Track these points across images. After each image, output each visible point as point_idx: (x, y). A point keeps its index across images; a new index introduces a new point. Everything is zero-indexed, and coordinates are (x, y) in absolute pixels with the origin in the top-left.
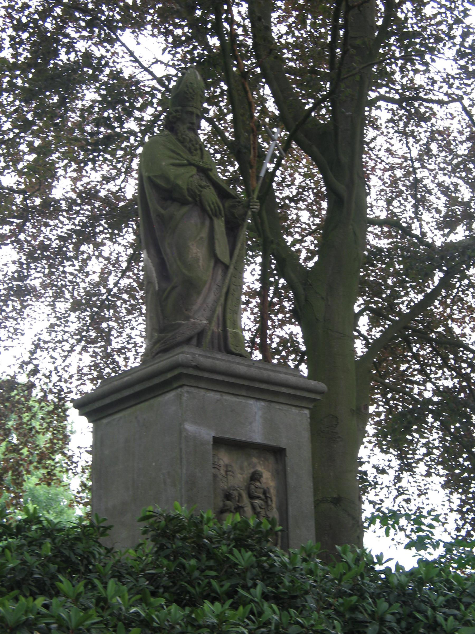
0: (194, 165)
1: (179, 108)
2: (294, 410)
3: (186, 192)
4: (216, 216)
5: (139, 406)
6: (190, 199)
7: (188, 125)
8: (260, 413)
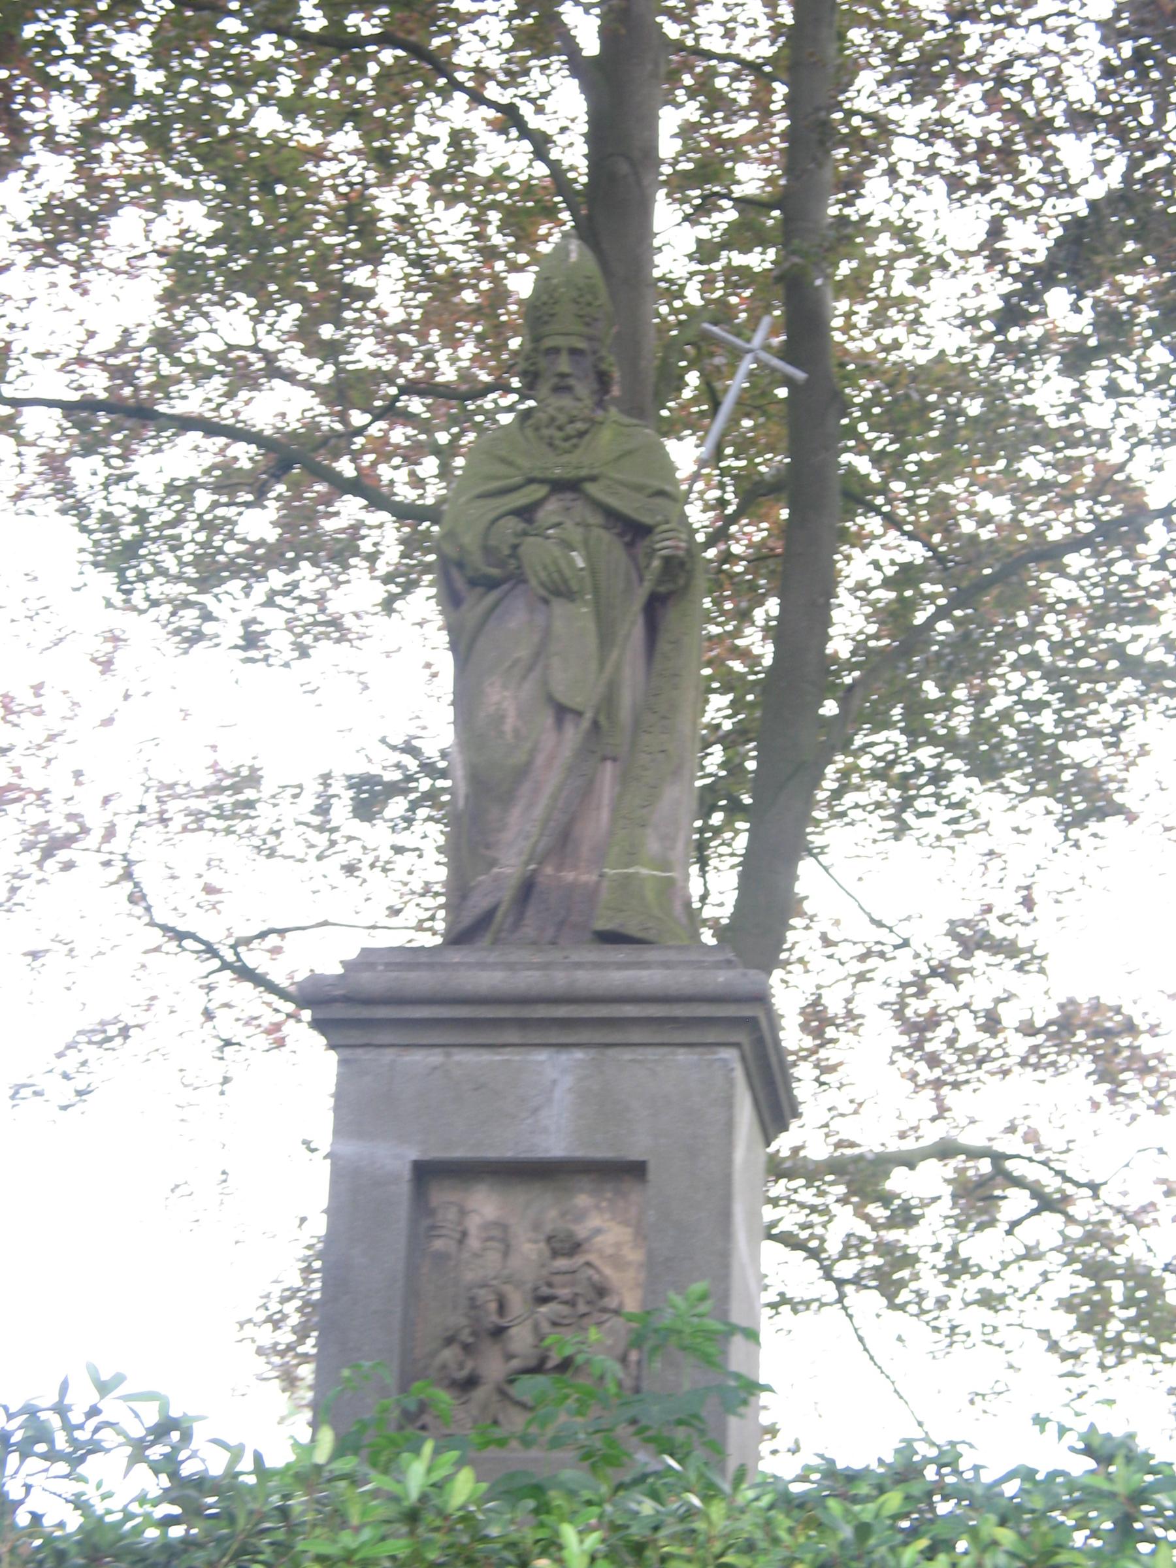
2: (683, 1056)
7: (555, 380)
8: (567, 1081)
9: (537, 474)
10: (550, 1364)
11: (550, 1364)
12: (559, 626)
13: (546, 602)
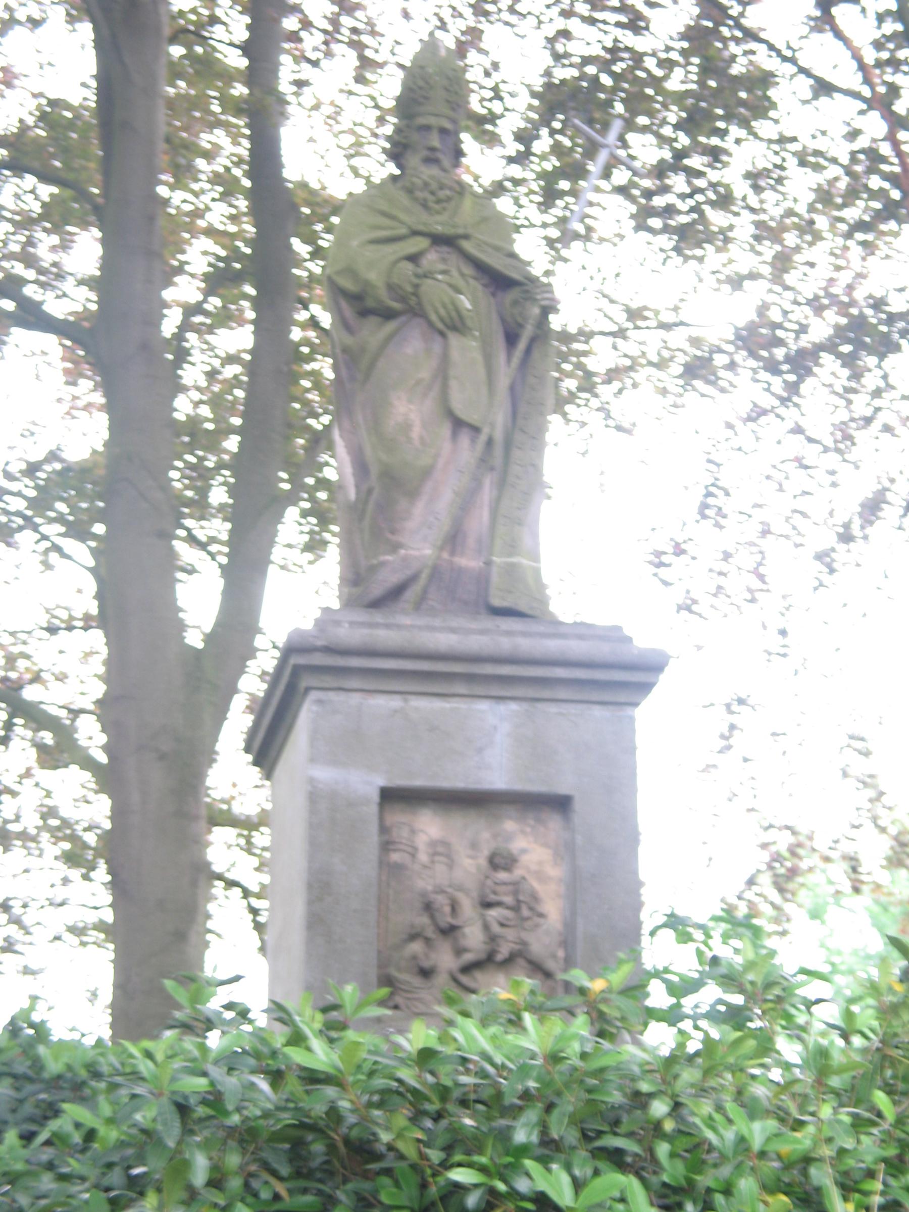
2: (598, 712)
7: (425, 153)
8: (505, 728)
9: (421, 228)
10: (499, 957)
11: (499, 957)
12: (455, 355)
13: (442, 334)
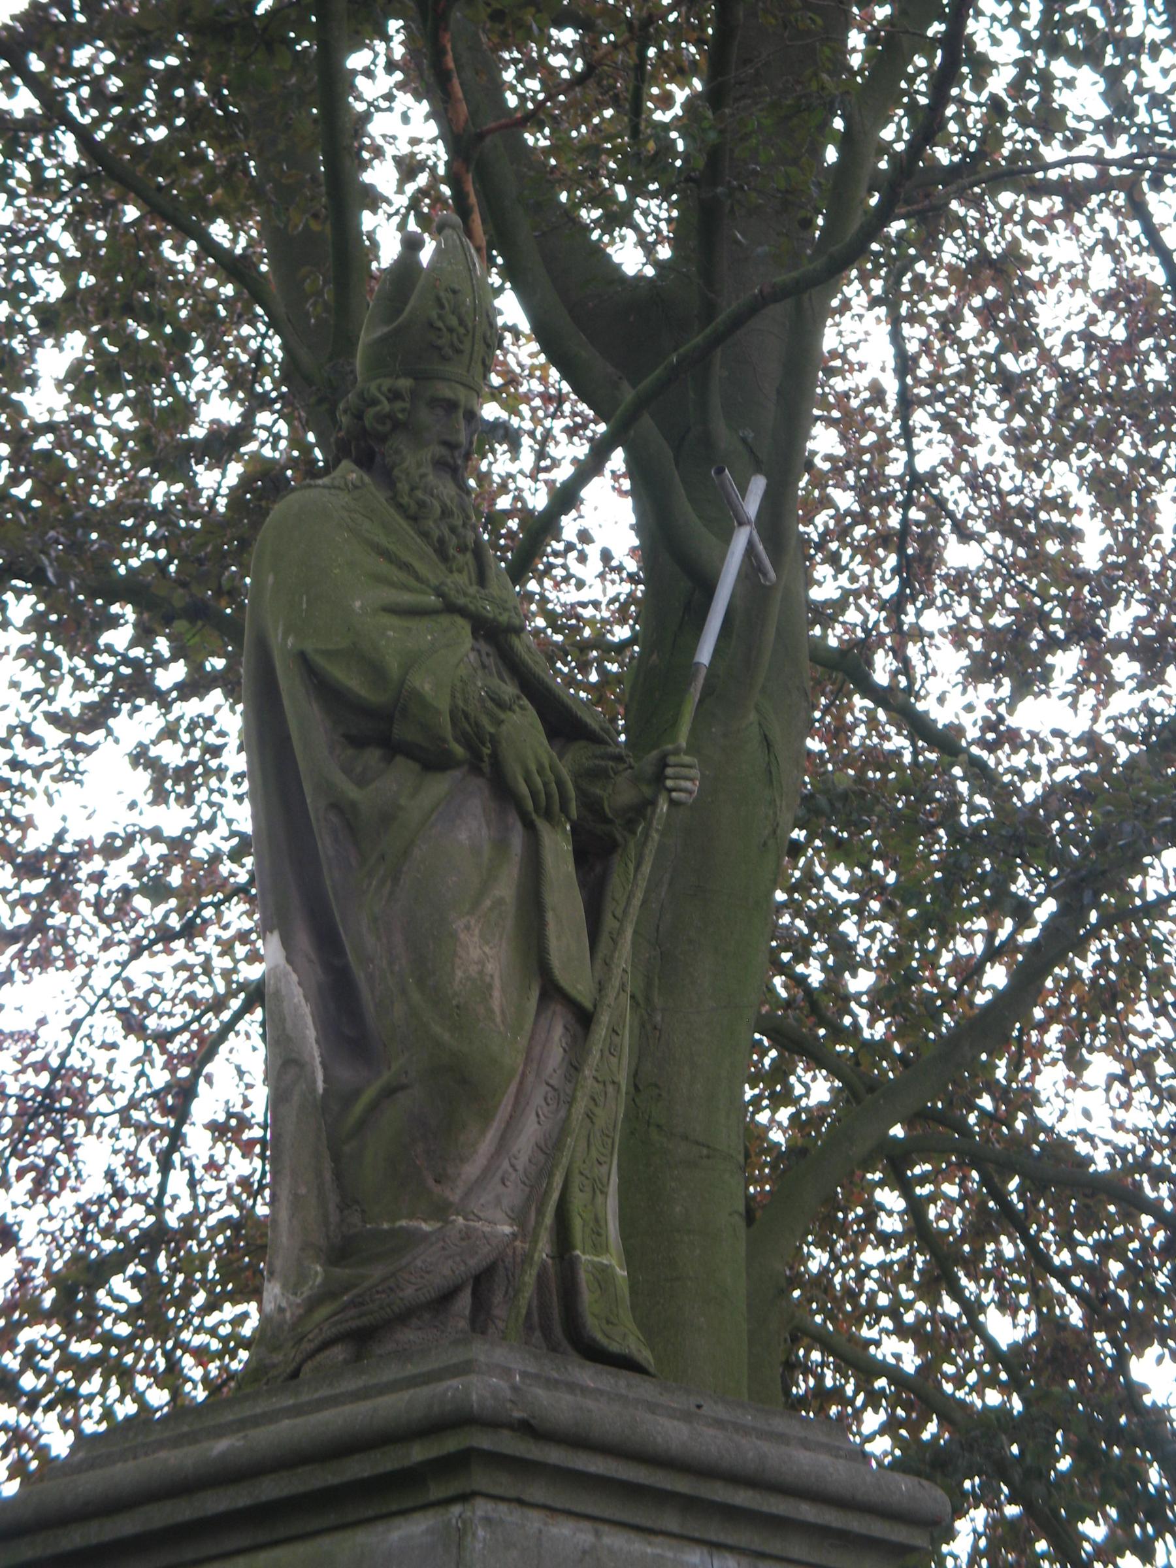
0: (463, 612)
1: (405, 383)
3: (448, 731)
4: (548, 815)
5: (263, 1557)
6: (459, 750)
